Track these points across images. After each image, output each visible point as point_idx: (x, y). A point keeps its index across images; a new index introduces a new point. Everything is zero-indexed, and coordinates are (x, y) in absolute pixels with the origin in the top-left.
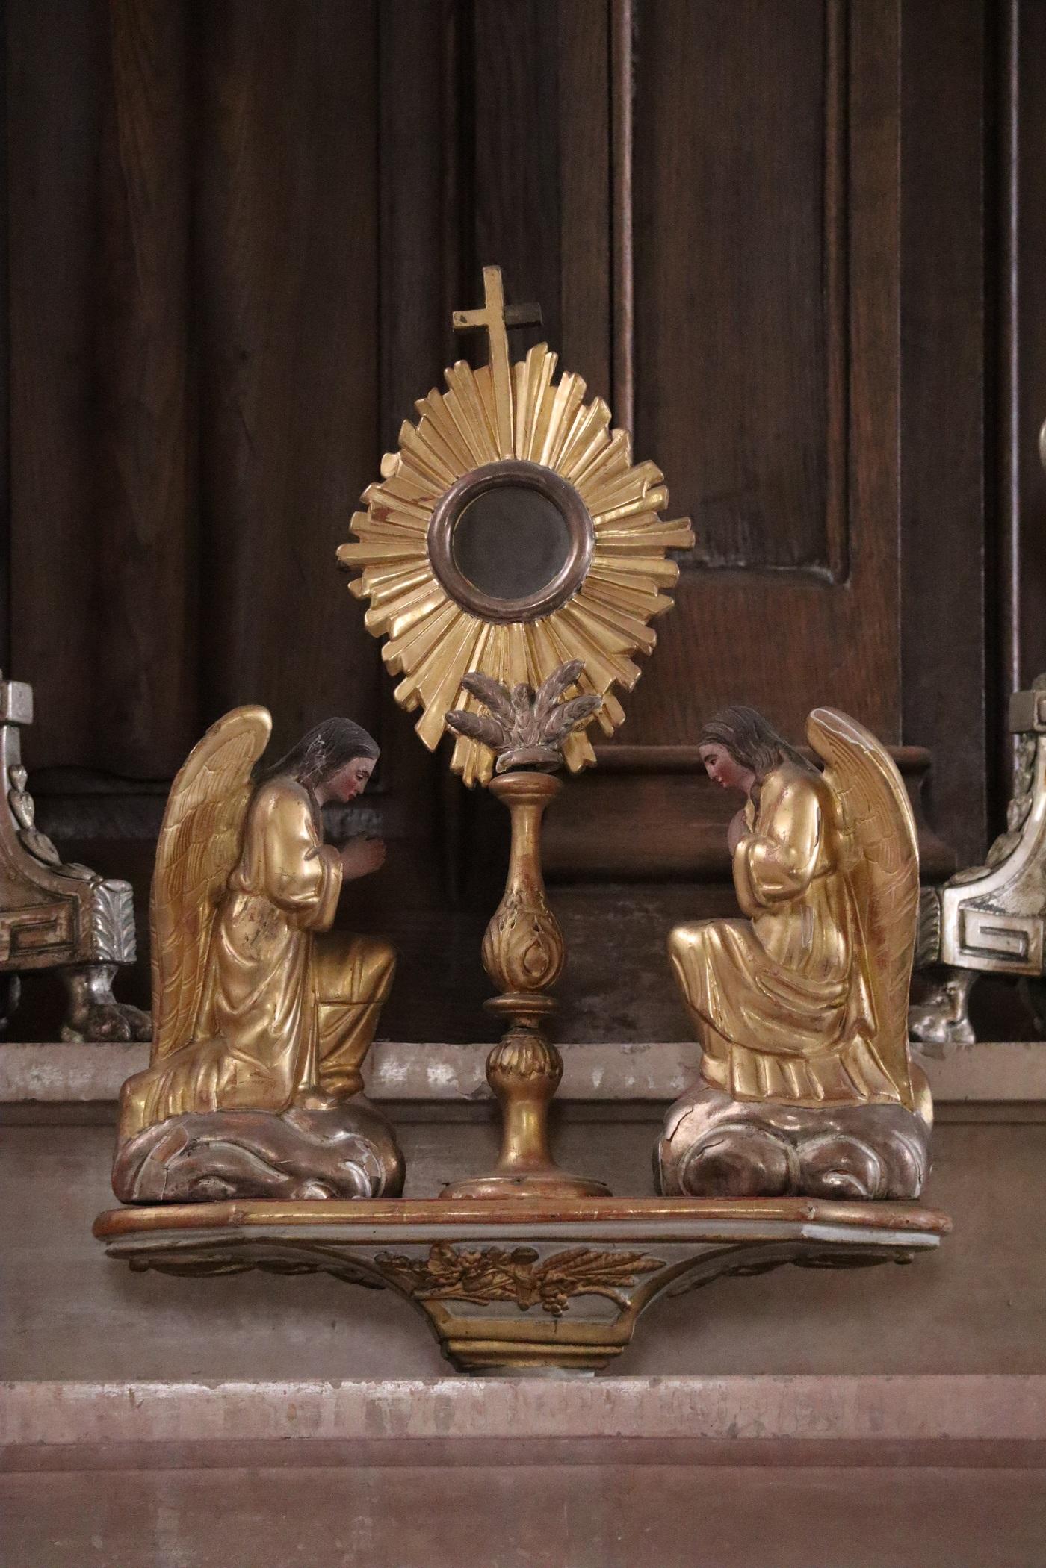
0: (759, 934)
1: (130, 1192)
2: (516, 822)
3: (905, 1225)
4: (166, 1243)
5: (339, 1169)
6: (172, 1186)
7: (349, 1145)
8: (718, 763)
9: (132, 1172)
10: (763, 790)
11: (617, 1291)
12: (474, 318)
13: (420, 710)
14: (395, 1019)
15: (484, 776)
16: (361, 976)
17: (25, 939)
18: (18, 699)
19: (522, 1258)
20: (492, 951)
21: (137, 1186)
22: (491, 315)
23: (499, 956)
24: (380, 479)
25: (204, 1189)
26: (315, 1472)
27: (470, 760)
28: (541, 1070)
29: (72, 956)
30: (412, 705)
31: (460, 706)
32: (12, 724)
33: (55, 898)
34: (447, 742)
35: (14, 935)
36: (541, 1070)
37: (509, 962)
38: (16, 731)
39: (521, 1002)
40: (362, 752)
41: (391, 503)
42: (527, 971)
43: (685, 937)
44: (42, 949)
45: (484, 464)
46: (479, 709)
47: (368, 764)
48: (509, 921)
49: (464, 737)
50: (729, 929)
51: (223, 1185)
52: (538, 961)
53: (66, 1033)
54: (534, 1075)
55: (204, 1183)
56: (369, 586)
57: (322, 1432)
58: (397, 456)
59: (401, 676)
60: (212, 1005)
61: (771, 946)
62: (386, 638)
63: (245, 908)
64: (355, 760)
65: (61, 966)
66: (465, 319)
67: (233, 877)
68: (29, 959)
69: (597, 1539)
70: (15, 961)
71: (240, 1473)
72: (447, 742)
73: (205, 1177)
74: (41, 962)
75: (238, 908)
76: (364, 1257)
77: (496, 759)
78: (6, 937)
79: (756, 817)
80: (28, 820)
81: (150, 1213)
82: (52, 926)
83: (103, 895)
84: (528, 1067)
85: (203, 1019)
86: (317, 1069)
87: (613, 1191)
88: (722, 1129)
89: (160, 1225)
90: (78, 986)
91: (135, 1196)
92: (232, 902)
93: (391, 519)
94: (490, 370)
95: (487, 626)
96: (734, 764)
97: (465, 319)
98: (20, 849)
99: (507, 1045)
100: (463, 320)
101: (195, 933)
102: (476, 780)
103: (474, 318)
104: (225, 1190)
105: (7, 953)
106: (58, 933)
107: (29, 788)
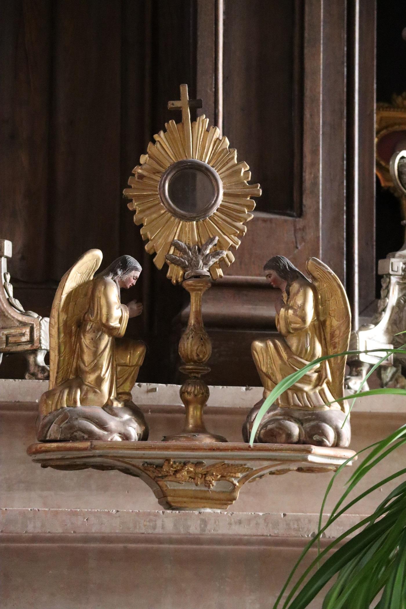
0: (289, 344)
1: (46, 437)
2: (192, 297)
3: (343, 457)
4: (60, 456)
5: (126, 430)
6: (63, 435)
7: (130, 420)
8: (272, 278)
9: (47, 429)
10: (291, 288)
11: (233, 479)
12: (177, 104)
13: (155, 254)
14: (150, 373)
15: (179, 280)
16: (136, 356)
17: (11, 339)
18: (8, 247)
19: (198, 464)
20: (184, 347)
21: (48, 434)
22: (183, 102)
23: (187, 349)
24: (141, 165)
25: (75, 436)
26: (149, 546)
27: (175, 274)
28: (203, 394)
29: (31, 346)
30: (151, 252)
31: (171, 252)
32: (7, 257)
33: (24, 324)
34: (166, 267)
35: (7, 338)
36: (203, 394)
37: (192, 352)
38: (6, 259)
39: (196, 367)
40: (136, 269)
41: (145, 173)
42: (198, 355)
43: (258, 345)
44: (19, 344)
45: (181, 160)
46: (178, 255)
47: (138, 274)
48: (191, 336)
49: (173, 265)
50: (277, 342)
51: (83, 434)
52: (201, 351)
53: (27, 376)
54: (200, 396)
55: (75, 434)
56: (135, 205)
57: (157, 531)
58: (147, 156)
59: (148, 240)
60: (77, 365)
61: (294, 348)
62: (142, 225)
63: (91, 327)
64: (133, 272)
65: (27, 350)
66: (173, 104)
67: (86, 315)
68: (14, 347)
69: (256, 575)
70: (8, 348)
71: (121, 545)
72: (166, 267)
73: (76, 431)
74: (20, 348)
75: (88, 327)
76: (137, 464)
77: (184, 273)
78: (4, 339)
79: (288, 298)
80: (11, 294)
81: (54, 445)
82: (23, 335)
83: (44, 323)
84: (198, 392)
85: (73, 370)
86: (117, 390)
87: (227, 439)
88: (274, 418)
89: (58, 449)
90: (31, 359)
91: (48, 438)
92: (86, 325)
93: (145, 180)
94: (183, 124)
95: (181, 222)
96: (279, 278)
97: (173, 104)
98: (8, 305)
99: (189, 384)
100: (173, 104)
101: (71, 337)
102: (177, 281)
103: (177, 104)
104: (83, 437)
105: (5, 345)
106: (26, 337)
107: (11, 282)
